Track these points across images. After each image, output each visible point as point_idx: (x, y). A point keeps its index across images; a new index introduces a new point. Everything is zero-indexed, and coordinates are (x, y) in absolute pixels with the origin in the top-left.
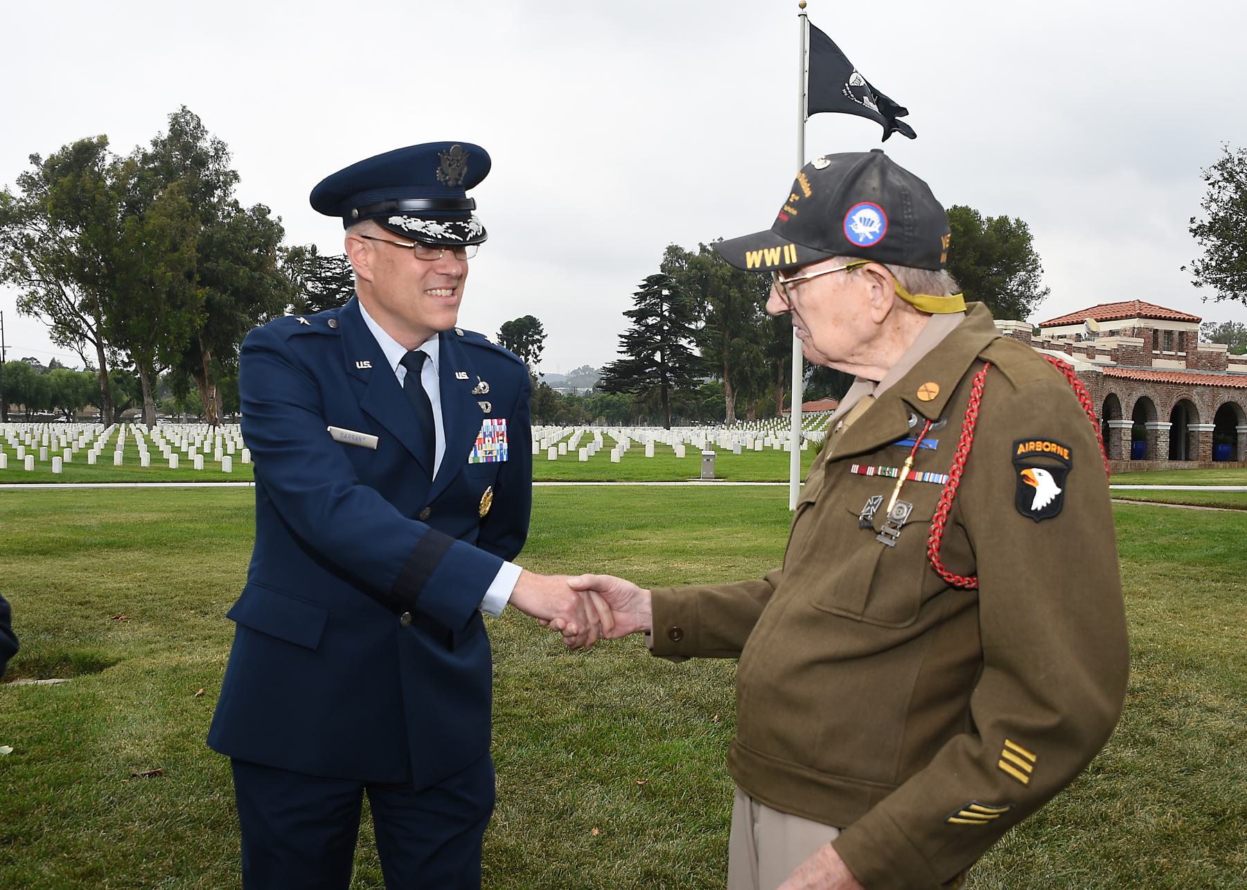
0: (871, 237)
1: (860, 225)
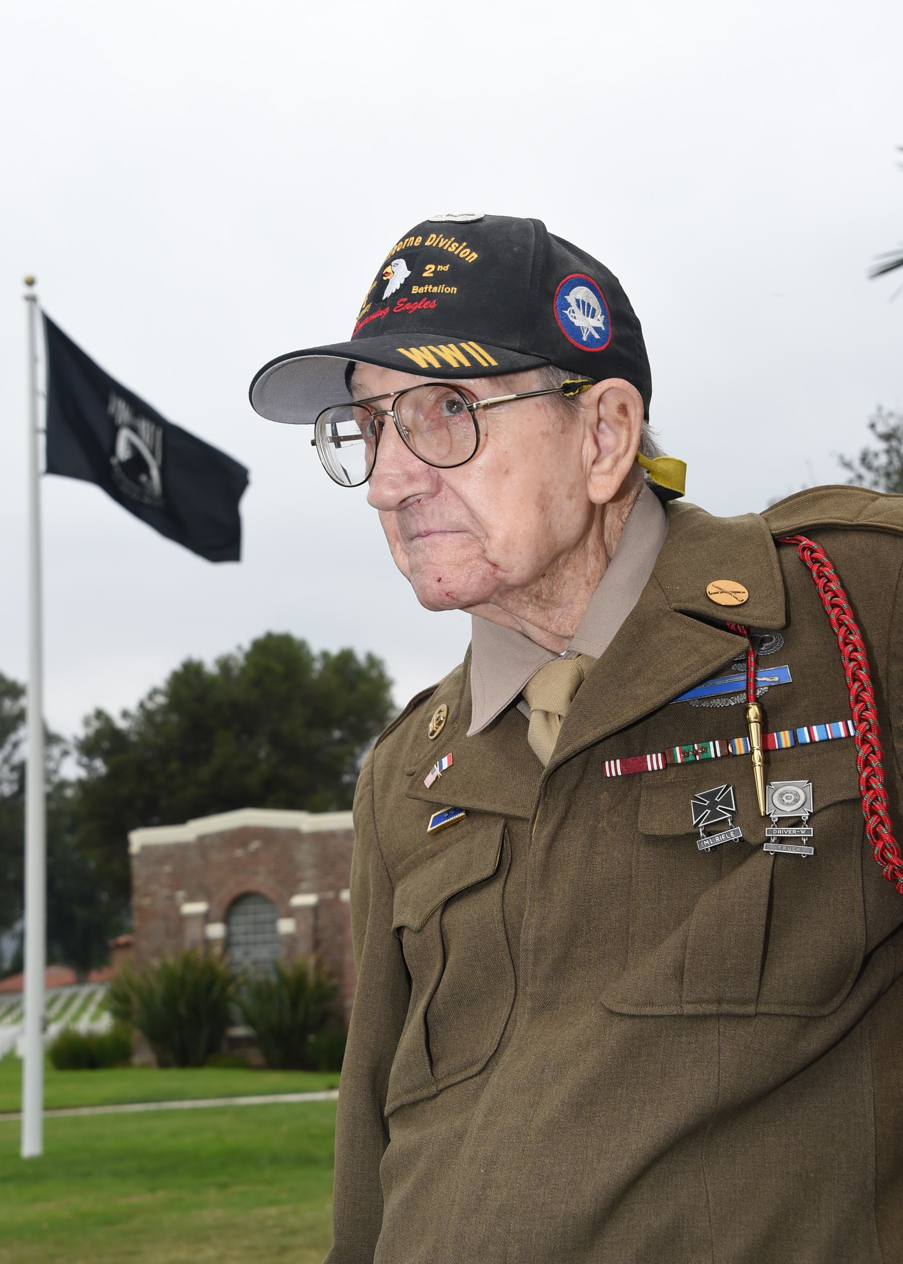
0: (597, 336)
1: (579, 313)
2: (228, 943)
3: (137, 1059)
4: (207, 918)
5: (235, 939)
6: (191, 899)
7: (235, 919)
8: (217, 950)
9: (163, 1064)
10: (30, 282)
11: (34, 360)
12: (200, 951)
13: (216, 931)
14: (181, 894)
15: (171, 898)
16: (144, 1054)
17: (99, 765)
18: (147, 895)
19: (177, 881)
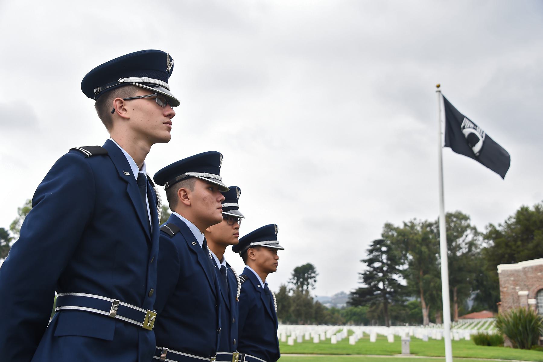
2: (537, 306)
3: (505, 344)
4: (528, 297)
5: (539, 305)
6: (522, 290)
7: (539, 298)
8: (533, 308)
9: (515, 347)
10: (438, 86)
11: (440, 111)
12: (527, 309)
13: (532, 301)
14: (517, 288)
15: (514, 289)
16: (508, 343)
17: (491, 242)
18: (505, 288)
19: (516, 283)
